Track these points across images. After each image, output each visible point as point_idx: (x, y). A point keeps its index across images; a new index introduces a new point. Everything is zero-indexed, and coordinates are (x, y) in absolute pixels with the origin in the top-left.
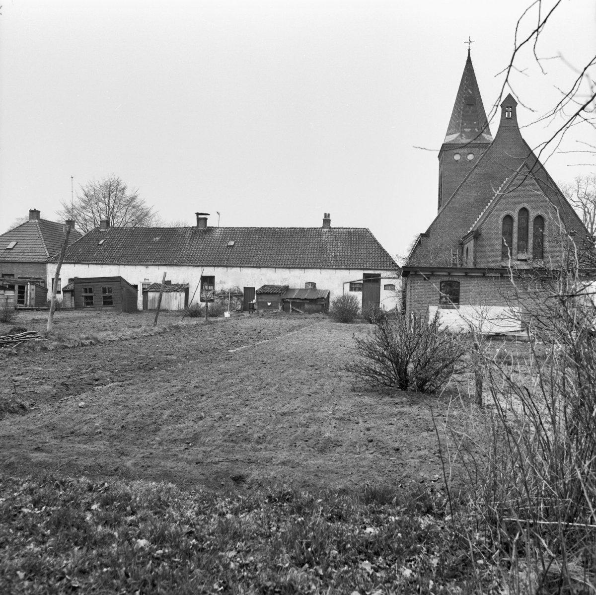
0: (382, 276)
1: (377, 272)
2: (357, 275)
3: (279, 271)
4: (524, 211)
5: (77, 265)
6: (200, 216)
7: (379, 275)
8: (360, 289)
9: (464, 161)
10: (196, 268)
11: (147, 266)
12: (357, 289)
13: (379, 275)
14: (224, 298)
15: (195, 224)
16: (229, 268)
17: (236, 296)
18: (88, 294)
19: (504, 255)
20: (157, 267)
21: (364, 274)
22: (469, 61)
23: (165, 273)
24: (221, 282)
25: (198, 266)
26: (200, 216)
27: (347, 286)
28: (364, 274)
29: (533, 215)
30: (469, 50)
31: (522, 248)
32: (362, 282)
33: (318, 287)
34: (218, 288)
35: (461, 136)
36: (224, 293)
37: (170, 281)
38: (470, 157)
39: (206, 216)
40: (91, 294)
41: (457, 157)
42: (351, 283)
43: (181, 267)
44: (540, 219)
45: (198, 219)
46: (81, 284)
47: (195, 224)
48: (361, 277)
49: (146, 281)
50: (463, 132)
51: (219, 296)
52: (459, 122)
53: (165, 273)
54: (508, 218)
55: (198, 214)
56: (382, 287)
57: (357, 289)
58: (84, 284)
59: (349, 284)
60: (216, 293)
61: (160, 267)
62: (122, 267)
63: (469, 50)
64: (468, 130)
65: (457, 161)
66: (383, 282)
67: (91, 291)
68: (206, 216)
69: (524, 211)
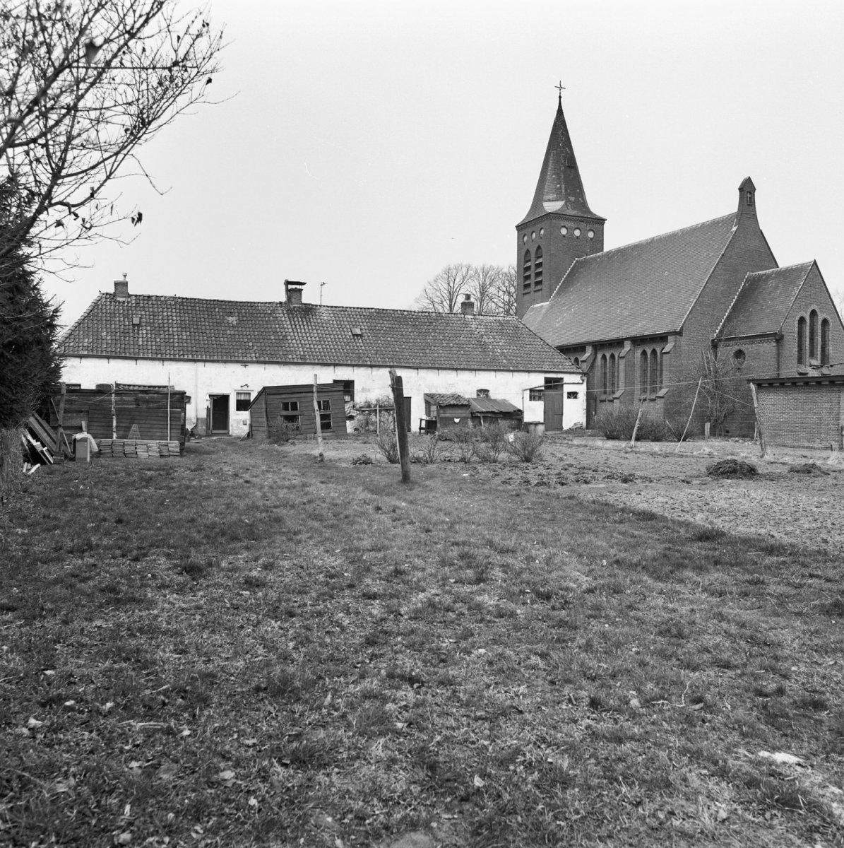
0: (565, 381)
1: (560, 376)
2: (538, 380)
3: (443, 374)
4: (813, 313)
5: (113, 362)
6: (290, 287)
7: (562, 379)
8: (540, 399)
9: (570, 237)
10: (325, 368)
11: (245, 363)
12: (537, 398)
13: (562, 379)
14: (369, 414)
15: (283, 298)
16: (374, 369)
17: (386, 410)
18: (290, 413)
19: (800, 360)
20: (263, 366)
21: (545, 378)
22: (560, 112)
23: (316, 375)
24: (363, 390)
25: (329, 365)
26: (290, 287)
27: (527, 394)
28: (545, 378)
29: (820, 318)
30: (560, 97)
31: (812, 355)
32: (543, 388)
33: (493, 395)
34: (360, 398)
35: (566, 205)
36: (369, 406)
37: (80, 385)
38: (577, 233)
39: (298, 287)
40: (295, 413)
41: (564, 231)
42: (531, 390)
43: (301, 367)
44: (825, 322)
45: (288, 291)
46: (279, 396)
47: (283, 298)
48: (542, 382)
49: (244, 388)
50: (567, 201)
51: (361, 410)
52: (560, 188)
53: (316, 375)
54: (802, 320)
55: (288, 283)
56: (565, 395)
57: (537, 398)
58: (284, 396)
59: (528, 392)
60: (358, 406)
61: (267, 366)
62: (200, 365)
63: (560, 97)
64: (572, 199)
65: (564, 236)
66: (567, 389)
67: (294, 406)
68: (298, 287)
69: (813, 313)
